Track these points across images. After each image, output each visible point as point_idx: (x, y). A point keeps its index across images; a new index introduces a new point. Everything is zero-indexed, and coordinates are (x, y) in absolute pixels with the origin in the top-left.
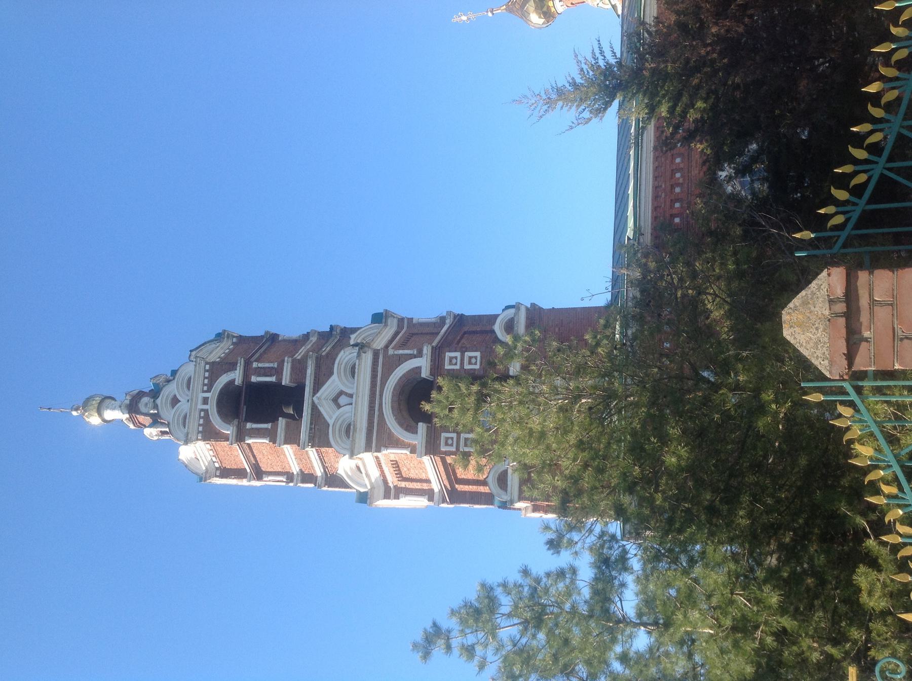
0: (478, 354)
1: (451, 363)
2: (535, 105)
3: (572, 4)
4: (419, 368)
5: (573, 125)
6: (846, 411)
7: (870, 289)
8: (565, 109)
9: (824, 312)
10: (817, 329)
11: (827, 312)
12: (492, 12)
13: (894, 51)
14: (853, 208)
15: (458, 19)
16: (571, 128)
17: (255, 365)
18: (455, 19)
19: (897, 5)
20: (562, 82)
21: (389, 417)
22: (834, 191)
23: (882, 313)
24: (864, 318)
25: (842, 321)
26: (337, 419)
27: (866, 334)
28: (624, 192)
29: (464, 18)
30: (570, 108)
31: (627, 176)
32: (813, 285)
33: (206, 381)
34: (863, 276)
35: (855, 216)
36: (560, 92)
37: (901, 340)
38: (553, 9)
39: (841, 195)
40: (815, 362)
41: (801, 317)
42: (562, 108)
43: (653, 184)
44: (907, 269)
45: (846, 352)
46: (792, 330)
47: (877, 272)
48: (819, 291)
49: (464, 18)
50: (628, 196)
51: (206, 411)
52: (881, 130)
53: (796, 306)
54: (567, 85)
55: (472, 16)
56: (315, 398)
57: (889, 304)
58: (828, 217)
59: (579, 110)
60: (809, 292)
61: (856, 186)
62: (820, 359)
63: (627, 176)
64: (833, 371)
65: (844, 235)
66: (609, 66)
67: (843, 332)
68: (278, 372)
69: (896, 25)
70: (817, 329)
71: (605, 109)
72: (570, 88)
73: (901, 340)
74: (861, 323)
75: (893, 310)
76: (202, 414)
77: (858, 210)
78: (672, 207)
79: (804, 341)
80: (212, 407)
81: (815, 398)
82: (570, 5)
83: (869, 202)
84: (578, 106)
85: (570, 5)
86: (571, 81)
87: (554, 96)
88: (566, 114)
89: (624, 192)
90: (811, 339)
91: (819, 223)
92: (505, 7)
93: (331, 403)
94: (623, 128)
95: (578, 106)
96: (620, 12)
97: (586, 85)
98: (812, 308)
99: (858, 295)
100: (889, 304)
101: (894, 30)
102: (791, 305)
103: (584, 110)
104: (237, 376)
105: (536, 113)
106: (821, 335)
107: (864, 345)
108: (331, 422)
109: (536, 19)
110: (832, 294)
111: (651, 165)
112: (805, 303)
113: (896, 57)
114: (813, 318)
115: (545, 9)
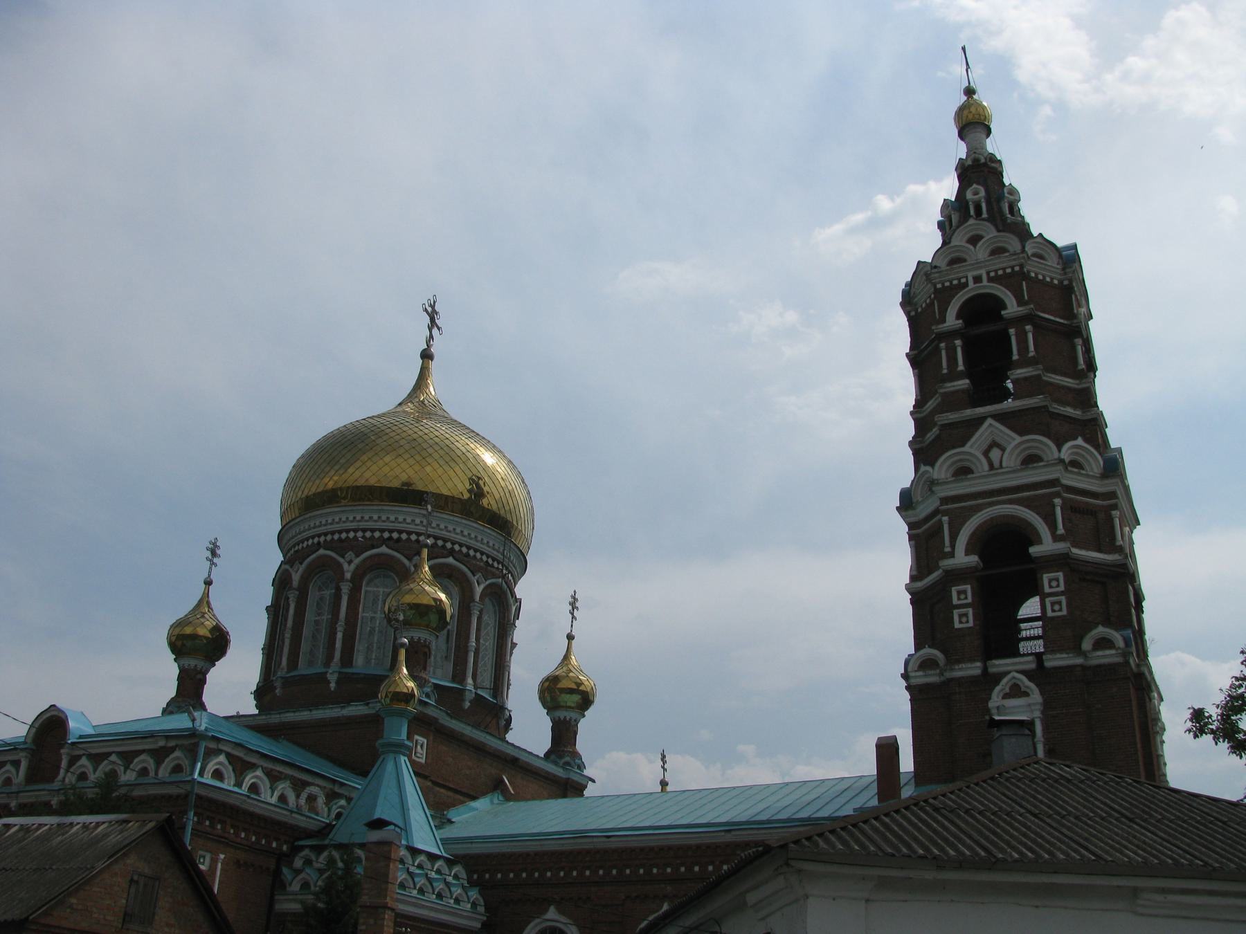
0: (1064, 612)
1: (965, 592)
4: (1039, 542)
17: (1028, 328)
18: (332, 689)
21: (980, 518)
26: (970, 454)
33: (1000, 272)
51: (966, 285)
56: (990, 421)
68: (1025, 362)
76: (963, 280)
80: (972, 289)
93: (988, 442)
104: (1012, 308)
108: (967, 448)
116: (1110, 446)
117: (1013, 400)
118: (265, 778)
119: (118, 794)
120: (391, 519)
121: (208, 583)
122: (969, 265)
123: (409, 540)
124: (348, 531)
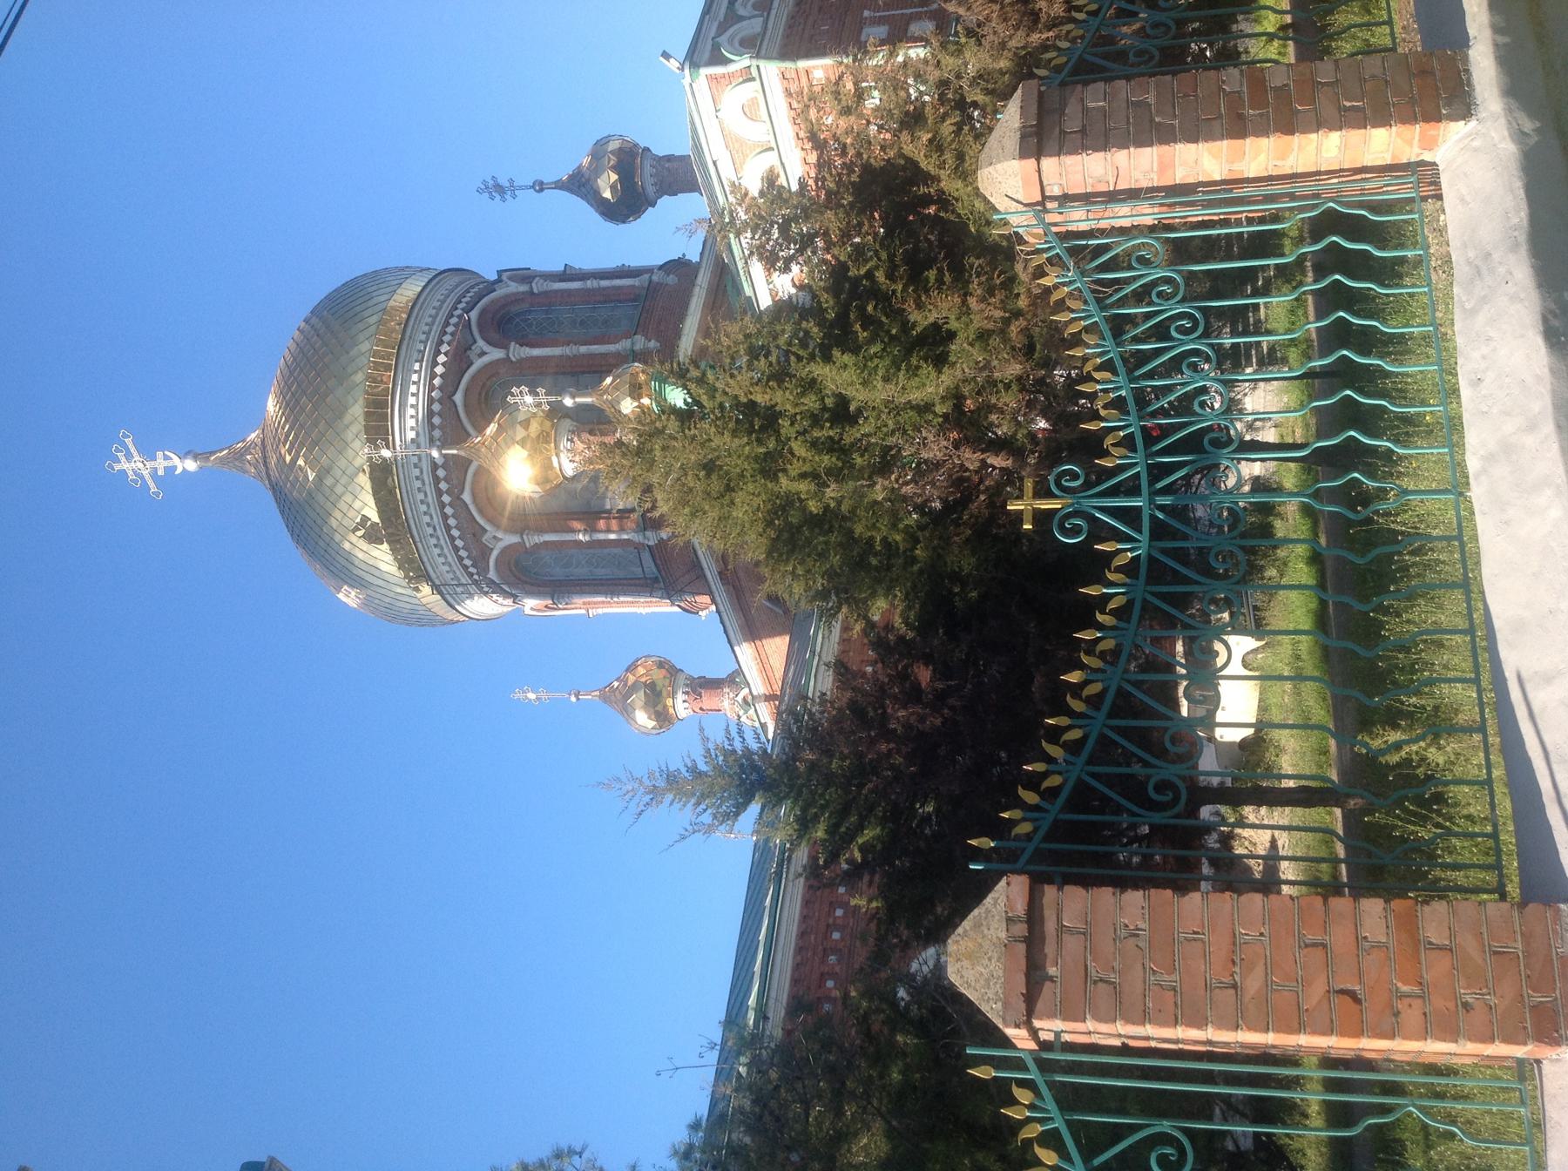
2: (631, 794)
3: (701, 709)
5: (687, 833)
6: (1024, 1096)
7: (1058, 909)
8: (677, 806)
9: (1000, 935)
10: (990, 959)
11: (1003, 935)
12: (577, 696)
13: (1098, 640)
14: (1043, 815)
15: (521, 696)
16: (683, 838)
19: (1105, 591)
20: (677, 764)
22: (1021, 791)
23: (1072, 944)
24: (1050, 949)
25: (1022, 948)
27: (1052, 971)
28: (741, 1004)
29: (532, 696)
30: (684, 806)
31: (750, 975)
32: (989, 900)
34: (1050, 892)
35: (1045, 827)
36: (672, 779)
37: (1095, 982)
38: (671, 710)
39: (1030, 797)
40: (984, 1008)
41: (970, 944)
42: (671, 804)
43: (792, 976)
44: (1103, 888)
45: (1024, 992)
46: (958, 965)
47: (1067, 888)
48: (995, 907)
49: (532, 696)
50: (753, 977)
52: (1080, 727)
53: (965, 931)
54: (684, 770)
55: (544, 696)
57: (1081, 933)
58: (1012, 823)
59: (697, 810)
60: (983, 911)
61: (1049, 789)
62: (991, 1002)
63: (755, 943)
64: (1008, 1018)
65: (1031, 847)
66: (748, 753)
67: (1023, 962)
69: (1103, 612)
70: (990, 959)
71: (737, 814)
72: (687, 775)
73: (1095, 982)
74: (1046, 955)
75: (1086, 940)
77: (1050, 818)
78: (823, 960)
79: (973, 979)
81: (982, 1073)
82: (698, 710)
83: (1062, 811)
84: (698, 804)
85: (698, 710)
86: (690, 765)
87: (661, 783)
88: (677, 815)
89: (741, 1004)
90: (981, 974)
91: (999, 829)
92: (597, 693)
94: (762, 852)
95: (698, 804)
96: (770, 736)
97: (711, 773)
98: (986, 931)
99: (1044, 932)
100: (1081, 933)
101: (1100, 618)
102: (960, 930)
103: (705, 810)
105: (633, 804)
106: (995, 967)
107: (1048, 985)
109: (643, 719)
110: (1012, 911)
111: (791, 959)
112: (977, 926)
113: (1101, 646)
114: (986, 944)
115: (659, 708)
116: (1050, 1041)
117: (1142, 767)
118: (731, 30)
119: (536, 538)
120: (418, 474)
121: (540, 187)
122: (659, 572)
123: (446, 479)
124: (461, 559)
